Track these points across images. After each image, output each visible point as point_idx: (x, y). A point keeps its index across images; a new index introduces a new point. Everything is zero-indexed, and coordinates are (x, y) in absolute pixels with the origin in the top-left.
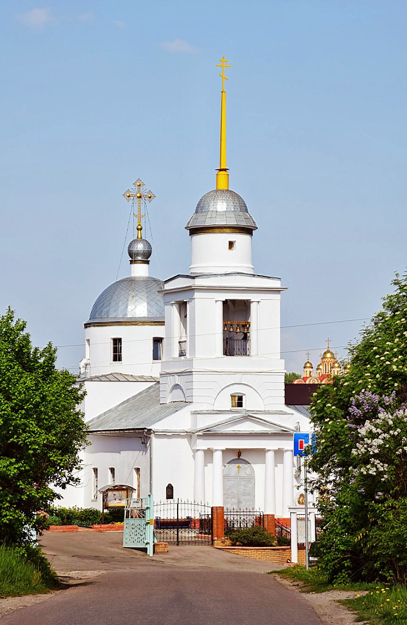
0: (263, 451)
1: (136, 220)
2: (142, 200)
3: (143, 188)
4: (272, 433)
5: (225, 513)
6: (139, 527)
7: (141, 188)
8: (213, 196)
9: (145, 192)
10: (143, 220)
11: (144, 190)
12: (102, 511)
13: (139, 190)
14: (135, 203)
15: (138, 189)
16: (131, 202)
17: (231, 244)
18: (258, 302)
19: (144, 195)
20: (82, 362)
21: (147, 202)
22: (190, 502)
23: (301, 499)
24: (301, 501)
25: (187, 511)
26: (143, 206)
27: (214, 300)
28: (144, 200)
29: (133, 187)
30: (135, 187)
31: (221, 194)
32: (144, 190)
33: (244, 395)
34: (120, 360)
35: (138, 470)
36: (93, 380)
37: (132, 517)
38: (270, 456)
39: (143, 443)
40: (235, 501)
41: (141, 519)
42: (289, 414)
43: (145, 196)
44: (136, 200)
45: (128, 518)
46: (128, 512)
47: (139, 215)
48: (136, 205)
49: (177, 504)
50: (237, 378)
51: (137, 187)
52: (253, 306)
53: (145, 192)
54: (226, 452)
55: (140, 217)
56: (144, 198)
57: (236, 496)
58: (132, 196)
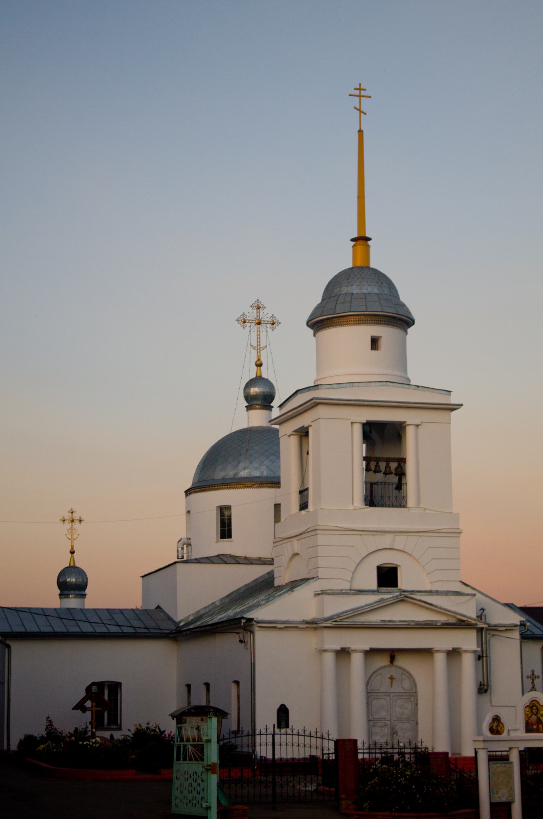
0: (428, 652)
1: (254, 353)
2: (262, 327)
3: (263, 311)
4: (443, 624)
5: (359, 751)
6: (195, 777)
7: (261, 312)
8: (347, 274)
9: (266, 317)
10: (263, 353)
11: (264, 314)
12: (321, 757)
13: (258, 314)
14: (252, 331)
15: (257, 313)
16: (247, 329)
17: (375, 343)
18: (417, 426)
19: (264, 321)
20: (180, 542)
21: (269, 330)
22: (307, 733)
23: (495, 724)
24: (494, 728)
25: (290, 748)
26: (263, 335)
27: (350, 421)
28: (265, 327)
29: (250, 310)
30: (253, 311)
31: (359, 271)
32: (264, 314)
33: (399, 566)
34: (230, 536)
35: (237, 683)
36: (188, 562)
37: (185, 759)
38: (440, 659)
39: (241, 641)
40: (386, 731)
41: (198, 762)
42: (468, 595)
43: (266, 322)
44: (255, 327)
45: (180, 760)
46: (179, 748)
47: (259, 347)
48: (254, 335)
49: (271, 736)
50: (386, 541)
51: (255, 311)
52: (410, 433)
53: (266, 317)
54: (371, 653)
55: (259, 349)
56: (265, 325)
57: (388, 723)
58: (249, 322)
